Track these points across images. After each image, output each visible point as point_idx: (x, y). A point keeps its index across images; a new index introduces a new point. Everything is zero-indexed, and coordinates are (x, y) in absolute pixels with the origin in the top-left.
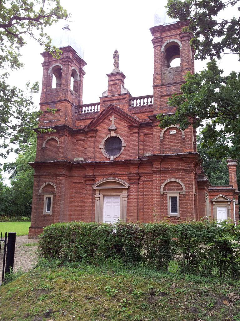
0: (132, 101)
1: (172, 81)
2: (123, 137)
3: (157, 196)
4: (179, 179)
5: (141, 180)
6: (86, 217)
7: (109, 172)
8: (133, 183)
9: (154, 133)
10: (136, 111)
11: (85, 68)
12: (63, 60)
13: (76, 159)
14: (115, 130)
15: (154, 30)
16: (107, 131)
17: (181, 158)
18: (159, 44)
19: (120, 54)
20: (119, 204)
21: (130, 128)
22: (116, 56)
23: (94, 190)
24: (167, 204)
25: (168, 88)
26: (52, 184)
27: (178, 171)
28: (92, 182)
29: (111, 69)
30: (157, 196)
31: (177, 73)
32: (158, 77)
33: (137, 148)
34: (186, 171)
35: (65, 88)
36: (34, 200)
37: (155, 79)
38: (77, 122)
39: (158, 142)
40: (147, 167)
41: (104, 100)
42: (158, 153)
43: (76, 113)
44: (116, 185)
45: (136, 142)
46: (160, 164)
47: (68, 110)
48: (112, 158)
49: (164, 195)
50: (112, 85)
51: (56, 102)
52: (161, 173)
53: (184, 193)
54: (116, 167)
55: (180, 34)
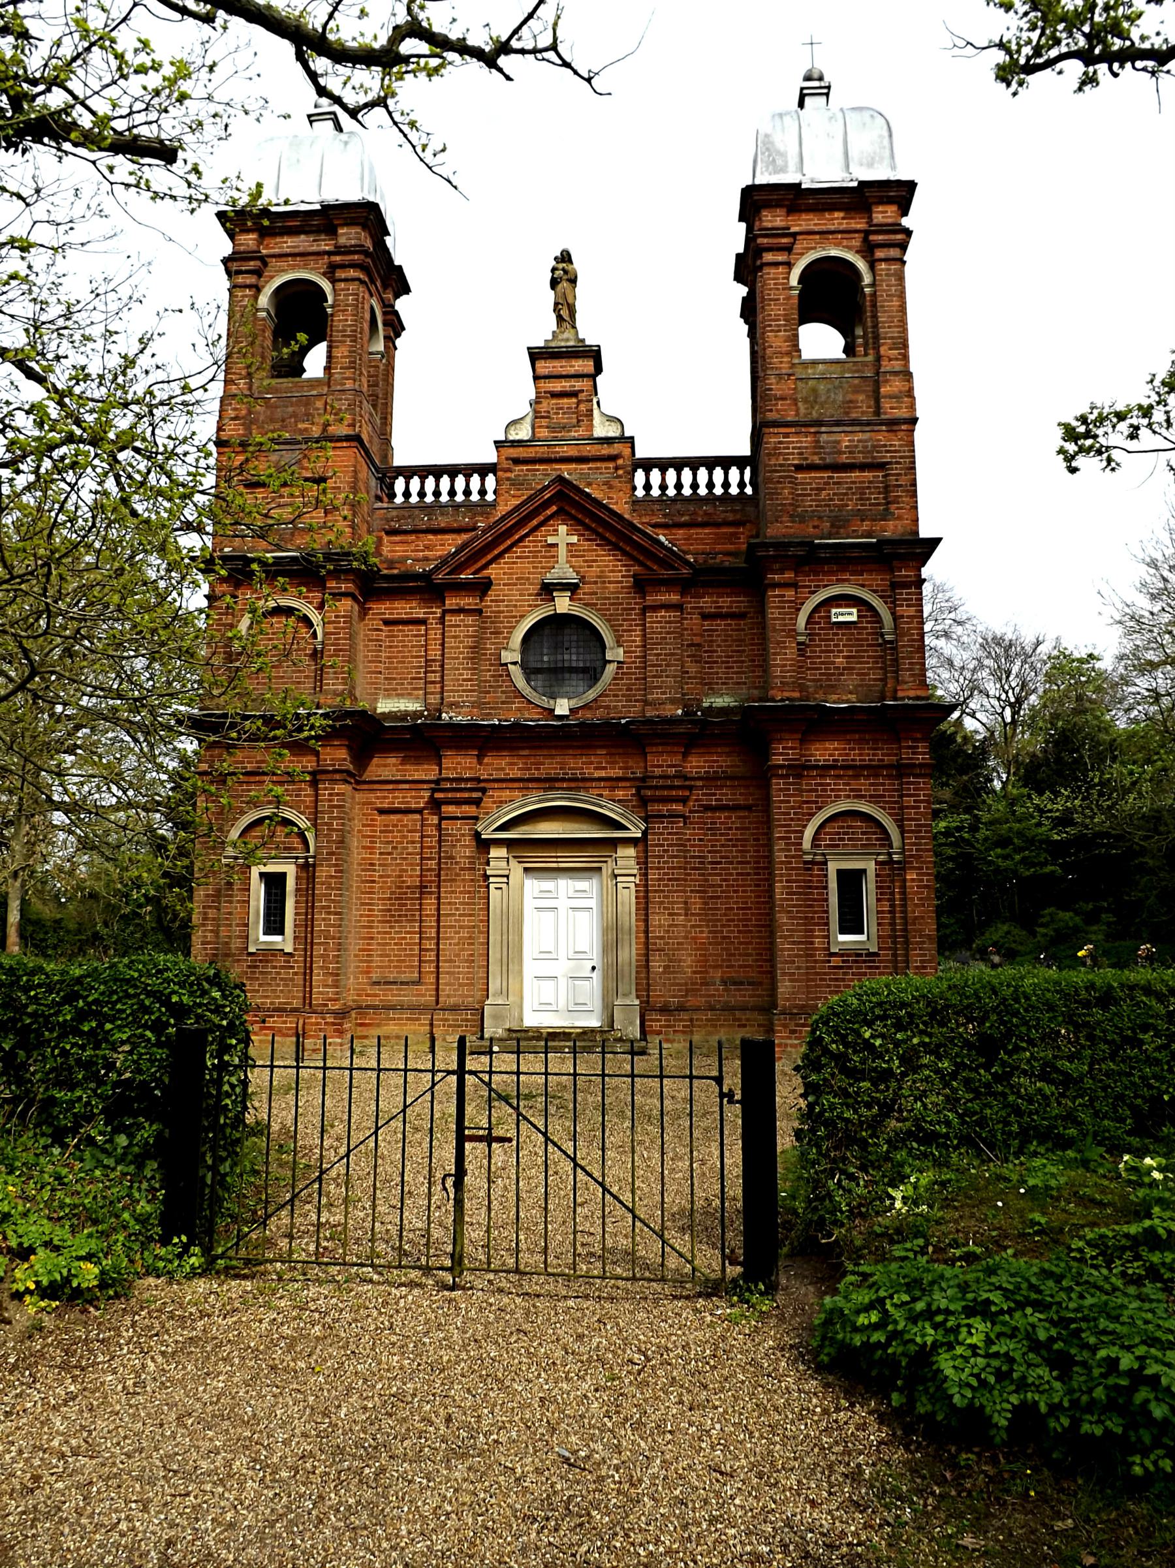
2: (608, 621)
3: (793, 869)
4: (875, 803)
6: (450, 961)
7: (550, 766)
8: (664, 816)
10: (665, 516)
11: (402, 305)
12: (338, 258)
13: (385, 706)
14: (573, 588)
15: (754, 201)
16: (534, 589)
18: (251, 280)
19: (578, 264)
20: (592, 903)
21: (640, 586)
22: (563, 276)
23: (484, 845)
24: (827, 900)
28: (470, 810)
29: (543, 330)
30: (793, 869)
31: (855, 386)
34: (901, 771)
39: (791, 652)
44: (576, 822)
48: (562, 707)
54: (579, 747)
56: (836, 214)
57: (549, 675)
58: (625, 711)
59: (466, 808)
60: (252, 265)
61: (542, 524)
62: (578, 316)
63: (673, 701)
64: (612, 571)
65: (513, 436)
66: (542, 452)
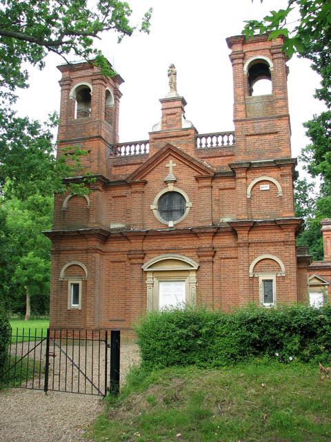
0: (198, 139)
1: (261, 115)
5: (216, 257)
7: (167, 244)
9: (238, 188)
11: (121, 88)
13: (113, 226)
17: (278, 225)
19: (177, 69)
22: (172, 73)
25: (256, 124)
26: (80, 264)
27: (274, 243)
28: (140, 261)
29: (166, 93)
32: (241, 108)
33: (209, 209)
35: (97, 119)
36: (52, 286)
37: (236, 111)
38: (113, 169)
39: (244, 202)
40: (226, 237)
41: (155, 137)
42: (244, 217)
43: (111, 155)
45: (208, 201)
46: (248, 234)
47: (102, 152)
48: (171, 224)
49: (254, 279)
50: (168, 115)
51: (84, 139)
52: (249, 247)
53: (284, 275)
55: (270, 49)
56: (260, 43)
57: (167, 212)
58: (191, 224)
59: (138, 260)
60: (67, 82)
61: (164, 160)
62: (177, 86)
63: (208, 221)
64: (187, 176)
65: (155, 130)
66: (163, 135)
